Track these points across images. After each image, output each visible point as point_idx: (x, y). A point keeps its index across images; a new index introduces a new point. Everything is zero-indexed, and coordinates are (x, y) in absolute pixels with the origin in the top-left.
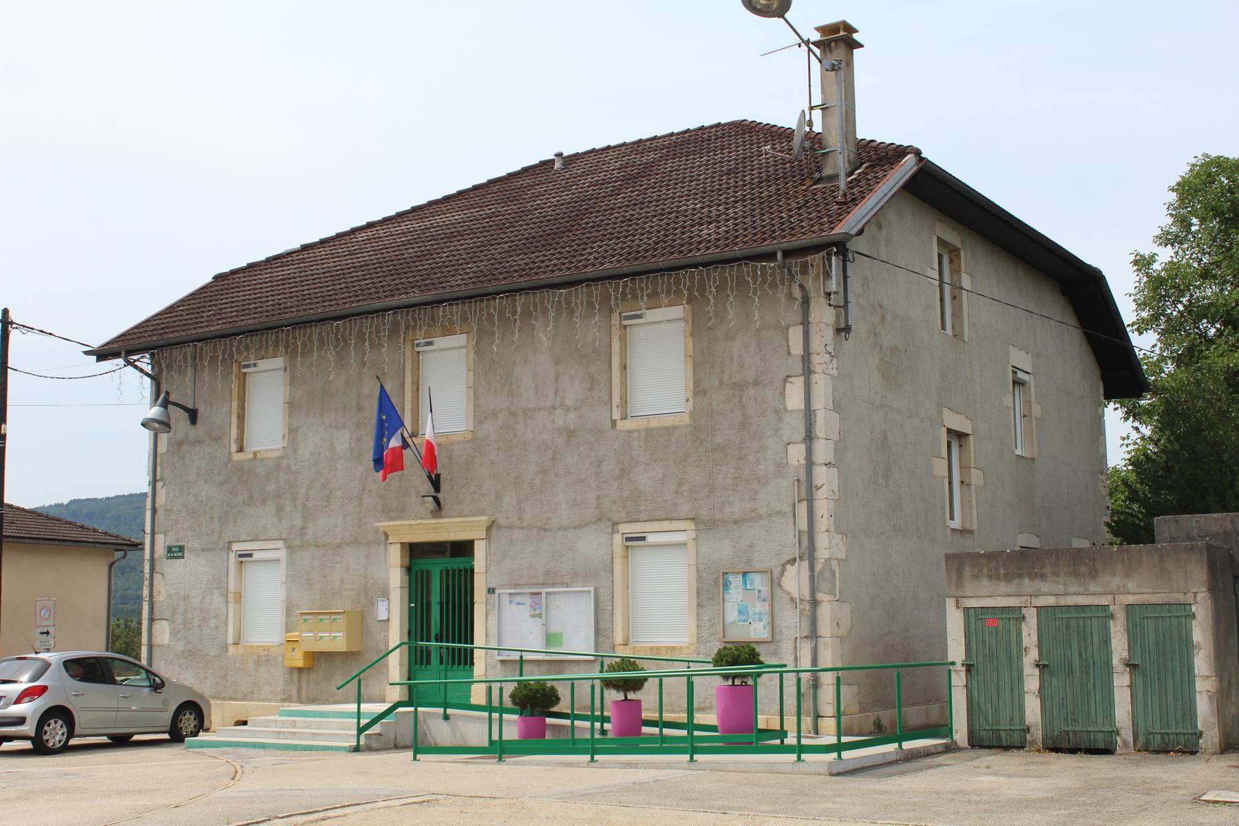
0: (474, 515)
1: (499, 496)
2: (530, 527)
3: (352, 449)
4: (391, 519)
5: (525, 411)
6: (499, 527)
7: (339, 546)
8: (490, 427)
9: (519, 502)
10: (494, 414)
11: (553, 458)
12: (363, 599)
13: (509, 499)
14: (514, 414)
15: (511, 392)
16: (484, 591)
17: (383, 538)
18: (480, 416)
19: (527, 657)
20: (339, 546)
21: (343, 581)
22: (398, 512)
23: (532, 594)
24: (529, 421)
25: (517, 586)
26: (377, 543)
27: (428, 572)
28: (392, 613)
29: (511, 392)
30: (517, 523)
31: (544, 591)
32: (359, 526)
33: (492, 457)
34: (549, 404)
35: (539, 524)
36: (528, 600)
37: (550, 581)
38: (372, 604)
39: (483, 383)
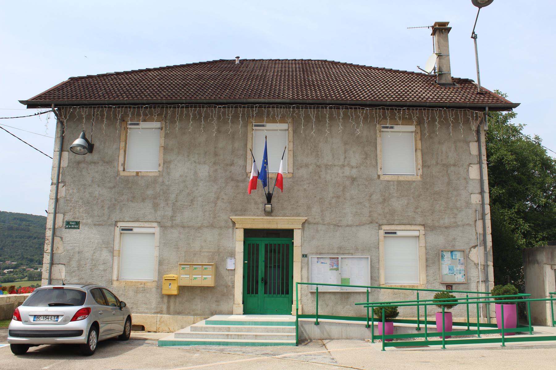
0: (293, 216)
1: (309, 207)
2: (329, 224)
3: (210, 176)
5: (327, 166)
7: (200, 228)
8: (303, 172)
9: (322, 211)
10: (307, 166)
11: (343, 191)
12: (216, 257)
13: (316, 210)
14: (319, 167)
15: (317, 155)
16: (301, 256)
17: (231, 225)
18: (297, 165)
19: (321, 289)
20: (200, 228)
21: (202, 247)
22: (243, 212)
23: (331, 258)
24: (329, 171)
25: (321, 254)
26: (228, 228)
27: (258, 246)
28: (236, 265)
29: (317, 155)
31: (340, 257)
32: (215, 218)
33: (305, 187)
34: (340, 163)
35: (335, 223)
36: (328, 261)
38: (224, 260)
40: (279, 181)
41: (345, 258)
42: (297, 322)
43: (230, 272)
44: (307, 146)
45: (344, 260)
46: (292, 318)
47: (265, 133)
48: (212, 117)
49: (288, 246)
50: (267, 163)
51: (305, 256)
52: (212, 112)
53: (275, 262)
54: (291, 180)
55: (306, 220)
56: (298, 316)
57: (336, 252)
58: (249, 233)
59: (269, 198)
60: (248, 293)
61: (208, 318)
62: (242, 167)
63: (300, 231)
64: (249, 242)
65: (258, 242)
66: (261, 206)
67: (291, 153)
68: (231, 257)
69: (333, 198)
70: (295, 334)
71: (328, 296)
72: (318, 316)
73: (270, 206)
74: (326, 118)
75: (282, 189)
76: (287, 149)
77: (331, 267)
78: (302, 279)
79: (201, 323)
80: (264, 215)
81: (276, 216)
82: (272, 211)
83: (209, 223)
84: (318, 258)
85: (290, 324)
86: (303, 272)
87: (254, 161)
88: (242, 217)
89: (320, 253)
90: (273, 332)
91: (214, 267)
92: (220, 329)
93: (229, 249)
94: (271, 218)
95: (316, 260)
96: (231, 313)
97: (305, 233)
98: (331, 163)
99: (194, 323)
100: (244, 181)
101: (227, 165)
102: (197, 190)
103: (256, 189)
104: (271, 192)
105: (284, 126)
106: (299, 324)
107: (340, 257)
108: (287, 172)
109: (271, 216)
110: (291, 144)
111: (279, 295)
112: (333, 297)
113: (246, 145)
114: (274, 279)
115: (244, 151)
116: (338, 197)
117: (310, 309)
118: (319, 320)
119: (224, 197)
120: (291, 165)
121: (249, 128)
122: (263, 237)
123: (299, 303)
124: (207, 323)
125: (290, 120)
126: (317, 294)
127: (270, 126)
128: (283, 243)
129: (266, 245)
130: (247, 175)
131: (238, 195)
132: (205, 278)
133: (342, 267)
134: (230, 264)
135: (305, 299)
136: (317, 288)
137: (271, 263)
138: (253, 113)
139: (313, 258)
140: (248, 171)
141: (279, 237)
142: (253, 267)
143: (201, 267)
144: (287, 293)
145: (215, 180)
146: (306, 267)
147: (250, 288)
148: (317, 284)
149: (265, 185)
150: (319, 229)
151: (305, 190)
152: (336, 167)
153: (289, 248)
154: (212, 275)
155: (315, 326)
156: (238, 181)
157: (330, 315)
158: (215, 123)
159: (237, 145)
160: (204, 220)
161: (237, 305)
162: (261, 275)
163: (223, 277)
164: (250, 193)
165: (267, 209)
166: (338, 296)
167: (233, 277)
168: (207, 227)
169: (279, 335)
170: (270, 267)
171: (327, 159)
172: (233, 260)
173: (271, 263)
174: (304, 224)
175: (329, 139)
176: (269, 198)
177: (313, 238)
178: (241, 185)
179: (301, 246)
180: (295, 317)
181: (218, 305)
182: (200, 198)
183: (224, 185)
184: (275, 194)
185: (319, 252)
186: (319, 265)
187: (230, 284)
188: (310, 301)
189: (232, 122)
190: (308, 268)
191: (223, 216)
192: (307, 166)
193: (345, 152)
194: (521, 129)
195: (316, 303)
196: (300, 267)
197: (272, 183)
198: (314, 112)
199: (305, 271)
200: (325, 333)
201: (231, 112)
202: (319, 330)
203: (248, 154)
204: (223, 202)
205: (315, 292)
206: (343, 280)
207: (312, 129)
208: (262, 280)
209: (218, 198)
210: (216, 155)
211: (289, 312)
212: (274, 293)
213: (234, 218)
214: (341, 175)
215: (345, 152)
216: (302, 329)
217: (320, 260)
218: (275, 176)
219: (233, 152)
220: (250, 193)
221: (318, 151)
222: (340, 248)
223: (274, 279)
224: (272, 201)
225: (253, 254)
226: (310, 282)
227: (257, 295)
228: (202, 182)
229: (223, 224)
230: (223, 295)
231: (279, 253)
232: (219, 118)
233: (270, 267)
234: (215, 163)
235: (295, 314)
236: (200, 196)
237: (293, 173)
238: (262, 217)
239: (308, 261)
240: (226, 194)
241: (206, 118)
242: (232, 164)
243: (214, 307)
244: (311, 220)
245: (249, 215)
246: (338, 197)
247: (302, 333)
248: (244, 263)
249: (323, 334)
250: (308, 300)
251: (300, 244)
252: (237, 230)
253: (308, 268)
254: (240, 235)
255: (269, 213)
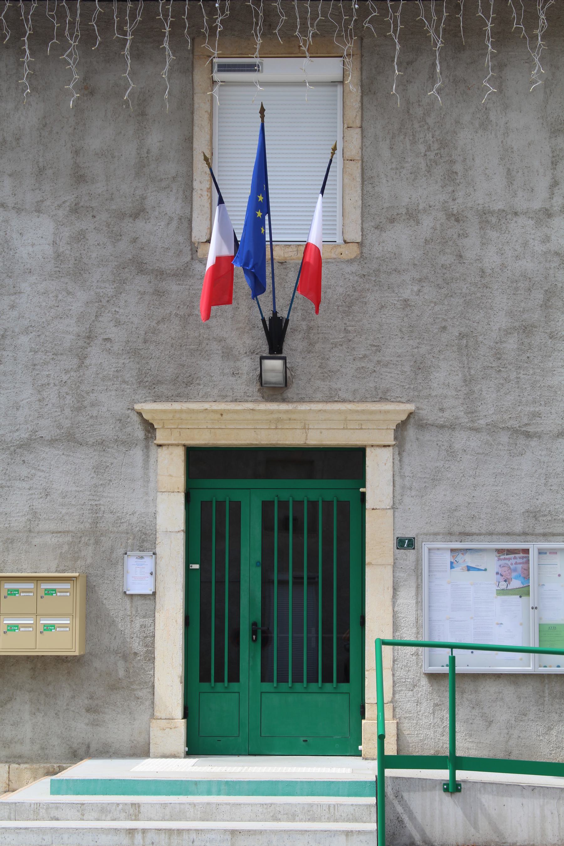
0: (363, 400)
1: (421, 368)
2: (493, 429)
3: (58, 256)
4: (157, 399)
5: (485, 216)
6: (422, 426)
7: (26, 445)
8: (399, 240)
9: (468, 381)
10: (412, 215)
11: (546, 305)
12: (88, 552)
13: (445, 376)
14: (458, 218)
15: (450, 177)
16: (391, 544)
17: (140, 434)
18: (376, 214)
19: (467, 662)
20: (26, 445)
21: (35, 514)
22: (183, 385)
23: (500, 551)
24: (493, 234)
25: (465, 535)
26: (127, 444)
27: (236, 507)
28: (160, 577)
29: (450, 177)
30: (464, 420)
31: (533, 547)
32: (79, 409)
33: (406, 293)
34: (537, 205)
35: (515, 424)
36: (492, 563)
37: (539, 530)
38: (114, 563)
39: (386, 153)
40: (311, 271)
41: (554, 552)
42: (380, 786)
43: (139, 602)
44: (414, 142)
45: (548, 559)
46: (364, 769)
47: (260, 94)
48: (61, 35)
49: (344, 507)
50: (265, 207)
51: (405, 543)
52: (61, 17)
53: (298, 565)
54: (354, 267)
55: (410, 415)
56: (386, 762)
57: (518, 528)
58: (203, 463)
59: (276, 333)
60: (204, 677)
61: (61, 769)
62: (174, 224)
63: (387, 454)
64: (205, 496)
65: (236, 496)
66: (247, 365)
67: (356, 169)
68: (141, 549)
69: (508, 332)
70: (373, 826)
71: (490, 689)
72: (456, 762)
73: (277, 364)
74: (481, 33)
75: (317, 302)
76: (339, 152)
77: (503, 585)
78: (396, 627)
79: (37, 791)
80: (257, 395)
81: (302, 400)
82: (286, 383)
83: (60, 427)
84: (452, 550)
85: (354, 788)
86: (400, 601)
87: (221, 201)
88: (177, 406)
89: (462, 536)
90: (293, 818)
91: (80, 585)
92: (104, 811)
93: (134, 519)
94: (284, 407)
95: (447, 557)
96: (143, 752)
97: (406, 460)
98: (500, 206)
99: (10, 789)
100: (183, 273)
101: (121, 216)
102: (13, 307)
103: (229, 302)
104: (282, 314)
105: (329, 68)
106: (389, 790)
107: (533, 547)
108: (339, 240)
109: (284, 400)
110: (355, 136)
111: (313, 687)
112: (509, 691)
113: (189, 140)
114: (298, 628)
115: (183, 163)
116: (527, 329)
117: (429, 736)
118: (461, 775)
119: (113, 332)
120: (355, 214)
121: (200, 77)
122: (256, 476)
123: (388, 713)
124: (56, 789)
125: (349, 46)
126: (452, 682)
127: (275, 68)
128: (329, 496)
129: (267, 506)
130: (195, 250)
131: (161, 327)
132: (48, 627)
133: (541, 585)
134: (137, 576)
135: (407, 701)
136: (453, 660)
137: (283, 568)
138: (212, 21)
139: (436, 554)
140: (198, 234)
141: (310, 476)
142: (220, 583)
143: (30, 586)
144: (345, 677)
145: (79, 272)
146: (412, 583)
147: (211, 659)
148: (452, 647)
149: (258, 287)
150: (457, 446)
151: (406, 303)
152: (521, 220)
153: (349, 517)
154: (72, 616)
155: (447, 799)
156: (161, 274)
157: (500, 756)
158: (72, 57)
159: (154, 139)
160: (41, 416)
161: (163, 723)
162: (249, 612)
163: (113, 623)
164: (208, 317)
165: (268, 377)
166: (527, 689)
167: (148, 621)
168: (52, 442)
169: (315, 832)
170: (283, 583)
171: (487, 188)
172: (148, 563)
173: (283, 568)
174: (401, 427)
175: (492, 116)
176: (276, 333)
177: (435, 479)
178: (173, 287)
179: (394, 508)
180: (374, 765)
181: (95, 724)
182: (24, 340)
183: (110, 290)
184: (295, 319)
185: (457, 529)
186: (459, 574)
187: (137, 646)
188: (426, 706)
189: (137, 55)
190: (419, 587)
191: (111, 403)
192: (412, 215)
193: (554, 164)
194: (258, 562)
195: (447, 715)
196: (390, 583)
197: (284, 282)
198: (439, 12)
199: (407, 598)
200: (483, 823)
201: (133, 17)
202: (460, 812)
203: (197, 176)
204: (109, 351)
205: (444, 675)
206: (544, 630)
207: (432, 78)
208: (254, 632)
209: (90, 337)
210: (79, 178)
211: (350, 747)
212: (298, 679)
213: (148, 408)
214: (539, 248)
215: (554, 164)
216: (399, 809)
217: (460, 558)
218: (295, 256)
219: (141, 167)
220: (208, 317)
221: (453, 162)
222: (534, 514)
223: (298, 628)
224: (285, 348)
225: (220, 536)
226: (425, 639)
227: (234, 686)
228: (33, 279)
229: (108, 430)
230: (114, 687)
231: (313, 530)
232: (88, 38)
233: (283, 583)
234: (75, 210)
235: (375, 752)
236: (26, 331)
237: (361, 244)
238: (250, 406)
239: (418, 561)
240: (118, 323)
241: (41, 38)
242: (139, 212)
243: (81, 729)
244: (429, 413)
245: (205, 398)
246: (527, 329)
247: (400, 821)
248: (188, 571)
249: (476, 827)
250: (418, 703)
251: (388, 502)
252: (163, 453)
253: (419, 587)
254: (171, 469)
255: (275, 391)
